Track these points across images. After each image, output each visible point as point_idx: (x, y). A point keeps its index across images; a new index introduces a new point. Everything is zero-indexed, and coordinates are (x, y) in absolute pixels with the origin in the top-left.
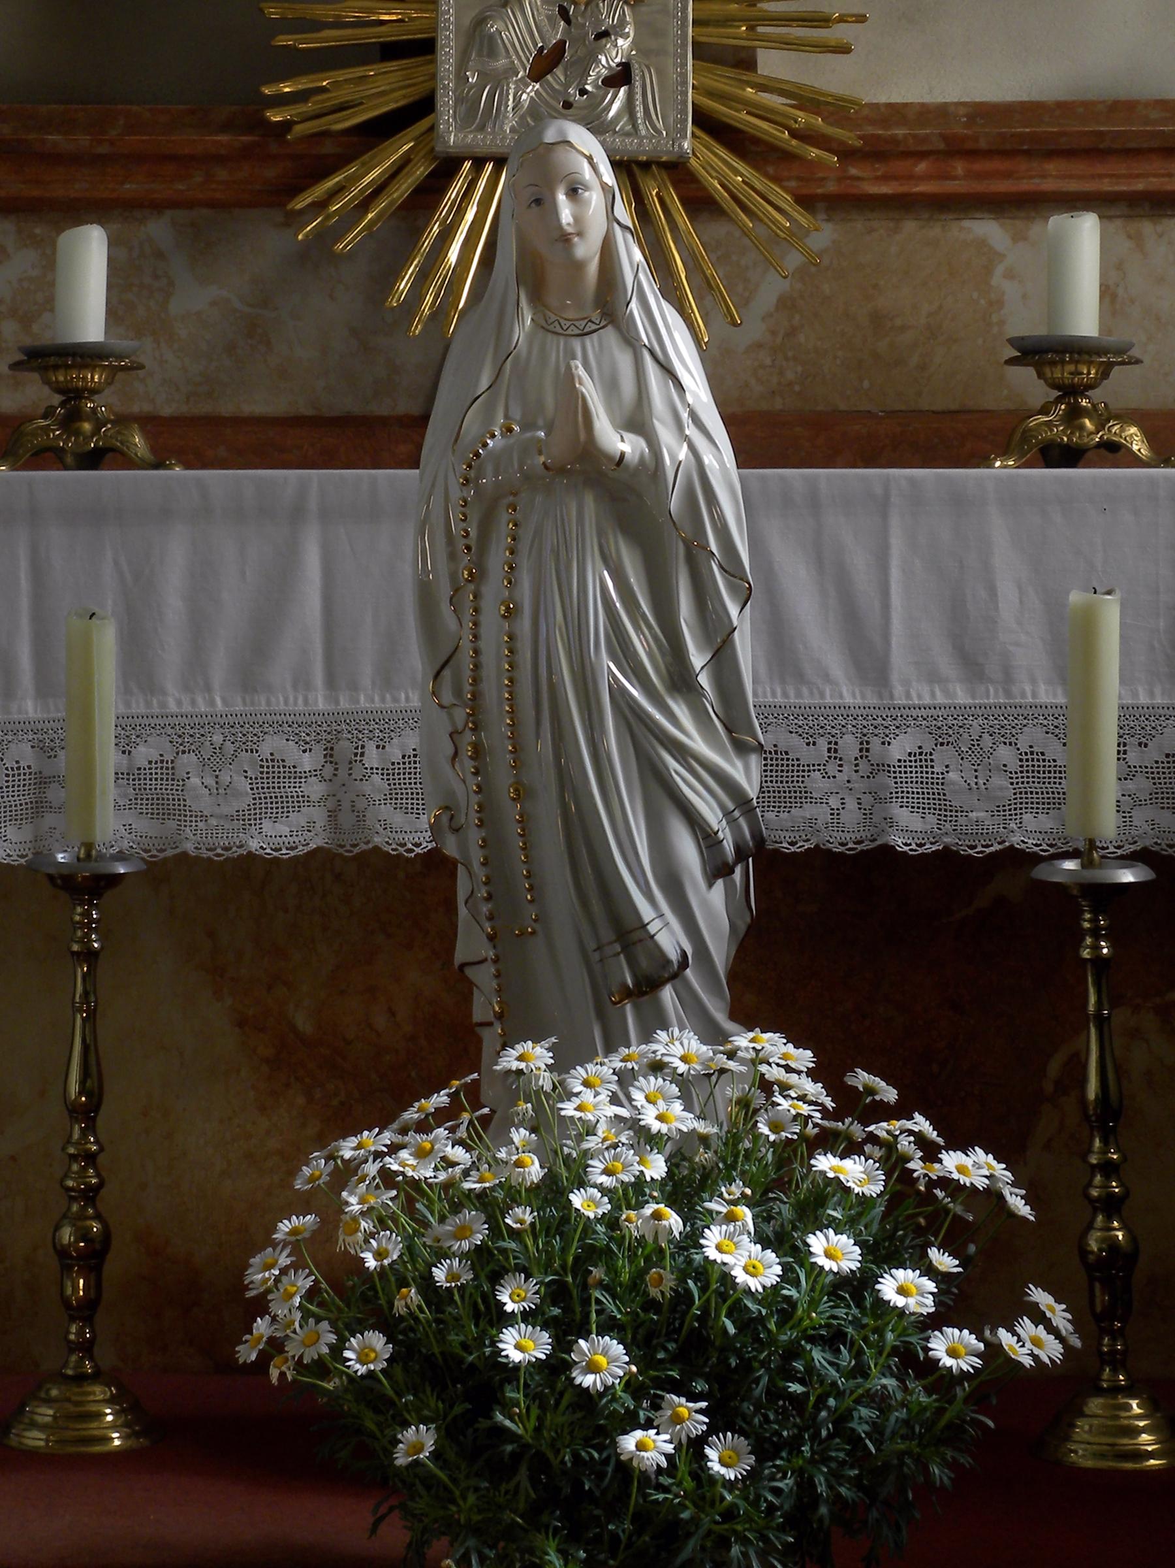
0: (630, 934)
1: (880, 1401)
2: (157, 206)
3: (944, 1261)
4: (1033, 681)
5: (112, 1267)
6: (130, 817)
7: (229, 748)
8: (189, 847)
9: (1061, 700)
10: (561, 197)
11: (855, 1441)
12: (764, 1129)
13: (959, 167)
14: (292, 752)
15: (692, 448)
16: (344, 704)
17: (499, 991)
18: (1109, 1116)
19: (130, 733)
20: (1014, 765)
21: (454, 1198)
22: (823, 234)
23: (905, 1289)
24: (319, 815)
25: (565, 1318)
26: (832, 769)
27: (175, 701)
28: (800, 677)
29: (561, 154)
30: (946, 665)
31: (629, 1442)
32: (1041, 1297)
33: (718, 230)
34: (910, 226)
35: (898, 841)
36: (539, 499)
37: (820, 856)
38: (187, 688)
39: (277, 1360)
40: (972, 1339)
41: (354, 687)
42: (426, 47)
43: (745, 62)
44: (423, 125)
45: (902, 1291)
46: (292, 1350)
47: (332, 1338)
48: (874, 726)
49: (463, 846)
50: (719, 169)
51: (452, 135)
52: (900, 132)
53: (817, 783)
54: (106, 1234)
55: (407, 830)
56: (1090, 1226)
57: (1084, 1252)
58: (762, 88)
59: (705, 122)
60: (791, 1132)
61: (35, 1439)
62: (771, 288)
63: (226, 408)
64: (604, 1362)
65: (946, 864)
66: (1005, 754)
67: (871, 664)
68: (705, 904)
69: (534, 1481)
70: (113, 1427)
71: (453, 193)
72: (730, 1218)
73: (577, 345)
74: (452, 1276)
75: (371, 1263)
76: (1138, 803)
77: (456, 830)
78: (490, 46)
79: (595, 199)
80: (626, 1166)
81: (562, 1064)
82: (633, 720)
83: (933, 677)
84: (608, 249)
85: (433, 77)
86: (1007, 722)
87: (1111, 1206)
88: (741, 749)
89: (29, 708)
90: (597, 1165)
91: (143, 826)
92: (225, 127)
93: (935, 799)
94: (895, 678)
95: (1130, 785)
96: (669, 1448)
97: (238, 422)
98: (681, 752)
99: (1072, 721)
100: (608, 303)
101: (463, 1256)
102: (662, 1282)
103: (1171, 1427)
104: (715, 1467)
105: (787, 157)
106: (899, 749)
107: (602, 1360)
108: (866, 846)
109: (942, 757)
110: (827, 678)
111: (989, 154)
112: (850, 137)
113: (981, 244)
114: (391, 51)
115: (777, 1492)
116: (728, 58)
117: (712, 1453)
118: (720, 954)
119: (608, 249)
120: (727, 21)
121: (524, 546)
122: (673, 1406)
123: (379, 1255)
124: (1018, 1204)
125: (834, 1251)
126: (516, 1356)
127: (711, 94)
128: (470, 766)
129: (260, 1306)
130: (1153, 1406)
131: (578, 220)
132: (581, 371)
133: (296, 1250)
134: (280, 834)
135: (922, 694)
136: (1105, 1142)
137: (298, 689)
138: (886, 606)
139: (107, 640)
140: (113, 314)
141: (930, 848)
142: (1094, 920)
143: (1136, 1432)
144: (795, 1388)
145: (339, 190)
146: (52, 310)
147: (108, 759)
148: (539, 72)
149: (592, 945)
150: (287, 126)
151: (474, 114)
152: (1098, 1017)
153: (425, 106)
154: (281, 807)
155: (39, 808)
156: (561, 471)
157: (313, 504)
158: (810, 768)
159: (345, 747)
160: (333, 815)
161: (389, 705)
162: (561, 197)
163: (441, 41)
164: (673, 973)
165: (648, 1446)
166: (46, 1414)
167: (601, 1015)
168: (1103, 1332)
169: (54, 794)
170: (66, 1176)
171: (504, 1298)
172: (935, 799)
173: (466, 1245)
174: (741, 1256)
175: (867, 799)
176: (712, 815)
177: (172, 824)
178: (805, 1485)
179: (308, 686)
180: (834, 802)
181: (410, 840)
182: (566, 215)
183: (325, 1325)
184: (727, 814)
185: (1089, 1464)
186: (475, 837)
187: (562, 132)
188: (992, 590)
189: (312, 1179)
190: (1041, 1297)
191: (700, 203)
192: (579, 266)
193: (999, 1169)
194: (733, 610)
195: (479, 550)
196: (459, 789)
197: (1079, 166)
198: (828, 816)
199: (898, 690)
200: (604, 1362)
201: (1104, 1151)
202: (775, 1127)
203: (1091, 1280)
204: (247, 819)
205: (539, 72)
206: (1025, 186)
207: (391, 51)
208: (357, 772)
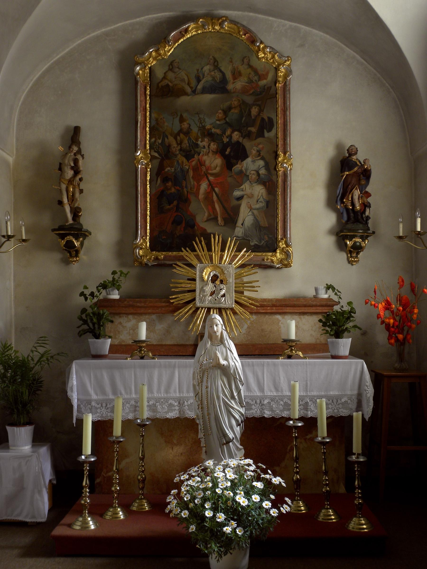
0: (225, 435)
1: (262, 519)
2: (154, 314)
3: (272, 497)
4: (286, 392)
5: (146, 482)
6: (149, 412)
7: (164, 402)
8: (158, 417)
9: (290, 394)
10: (215, 326)
11: (259, 525)
12: (245, 477)
13: (274, 308)
14: (173, 402)
15: (234, 363)
16: (181, 395)
17: (205, 443)
18: (297, 459)
19: (149, 400)
20: (283, 404)
21: (198, 488)
22: (254, 317)
23: (267, 504)
24: (178, 412)
25: (215, 509)
26: (256, 405)
27: (156, 395)
28: (251, 391)
29: (215, 319)
30: (273, 389)
31: (225, 529)
32: (287, 499)
33: (237, 317)
34: (267, 316)
35: (266, 416)
36: (211, 370)
37: (254, 418)
38: (157, 393)
39: (171, 513)
40: (276, 511)
41: (183, 393)
42: (194, 291)
43: (242, 293)
44: (194, 302)
45: (266, 505)
46: (174, 512)
47: (180, 510)
48: (262, 398)
49: (200, 422)
50: (238, 309)
51: (198, 304)
52: (265, 303)
53: (253, 407)
54: (145, 477)
55: (191, 414)
56: (294, 476)
57: (293, 479)
58: (245, 297)
59: (236, 302)
60: (250, 477)
61: (134, 509)
62: (246, 326)
63: (164, 343)
64: (221, 517)
65: (273, 419)
66: (282, 402)
67: (262, 389)
68: (236, 430)
69: (210, 532)
70: (147, 506)
71: (198, 313)
72: (240, 494)
73: (217, 347)
74: (198, 502)
75: (186, 499)
76: (301, 410)
77: (198, 419)
78: (204, 291)
79: (220, 326)
80: (224, 485)
81: (215, 465)
82: (225, 404)
83: (271, 391)
84: (222, 333)
85: (195, 295)
86: (282, 398)
87: (297, 473)
88: (242, 407)
89: (134, 396)
90: (220, 484)
91: (151, 414)
92: (164, 302)
93: (272, 410)
94: (265, 391)
95: (300, 407)
96: (231, 530)
97: (165, 345)
98: (233, 408)
99: (292, 398)
100: (222, 341)
101: (199, 498)
102: (230, 503)
103: (306, 505)
104: (238, 532)
105: (248, 307)
106: (266, 402)
107: (221, 517)
108: (261, 416)
109: (272, 403)
110: (255, 391)
111: (278, 306)
112: (257, 304)
113: (278, 319)
114: (189, 291)
115: (247, 534)
116: (240, 292)
117: (237, 530)
118: (238, 437)
119: (222, 333)
120: (239, 287)
121: (209, 378)
122: (232, 523)
123: (187, 498)
124: (284, 485)
125: (256, 498)
126: (208, 516)
127: (237, 298)
128: (201, 410)
129: (169, 503)
130: (303, 502)
131: (217, 330)
132: (218, 353)
133: (174, 496)
134: (171, 415)
135: (269, 394)
136: (296, 463)
137: (175, 393)
138: (264, 381)
139: (146, 388)
140: (147, 336)
141: (270, 417)
142: (295, 431)
143: (301, 507)
144: (250, 518)
145: (181, 312)
146: (138, 329)
147: (146, 403)
148: (211, 295)
149: (219, 437)
150: (173, 302)
151: (202, 301)
152: (295, 445)
153: (194, 299)
154: (172, 411)
155: (135, 411)
156: (215, 366)
157: (177, 366)
158: (252, 405)
159: (182, 402)
160: (180, 412)
161: (188, 395)
162: (215, 326)
163: (197, 290)
164: (231, 441)
165: (228, 529)
166: (136, 505)
167: (221, 447)
168: (296, 491)
169: (137, 409)
170: (139, 469)
171: (206, 506)
172: (272, 410)
173: (200, 497)
174: (242, 500)
175: (261, 409)
176: (237, 417)
177: (155, 413)
178: (251, 532)
179: (176, 392)
180: (256, 410)
181: (191, 416)
182: (215, 328)
183: (179, 508)
184: (240, 416)
185: (294, 512)
186: (201, 421)
187: (215, 316)
188: (280, 378)
189: (177, 480)
190: (287, 499)
191: (235, 313)
192: (218, 336)
193: (281, 480)
194: (241, 387)
195: (202, 378)
196: (199, 414)
197: (292, 308)
198: (255, 412)
199: (266, 393)
200: (221, 517)
201: (296, 465)
202: (247, 477)
203: (294, 484)
204: (167, 413)
205: (211, 295)
206: (284, 311)
207: (189, 291)
208: (183, 406)
